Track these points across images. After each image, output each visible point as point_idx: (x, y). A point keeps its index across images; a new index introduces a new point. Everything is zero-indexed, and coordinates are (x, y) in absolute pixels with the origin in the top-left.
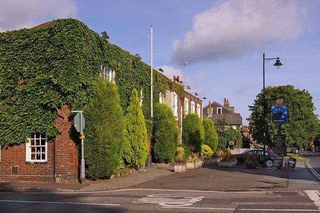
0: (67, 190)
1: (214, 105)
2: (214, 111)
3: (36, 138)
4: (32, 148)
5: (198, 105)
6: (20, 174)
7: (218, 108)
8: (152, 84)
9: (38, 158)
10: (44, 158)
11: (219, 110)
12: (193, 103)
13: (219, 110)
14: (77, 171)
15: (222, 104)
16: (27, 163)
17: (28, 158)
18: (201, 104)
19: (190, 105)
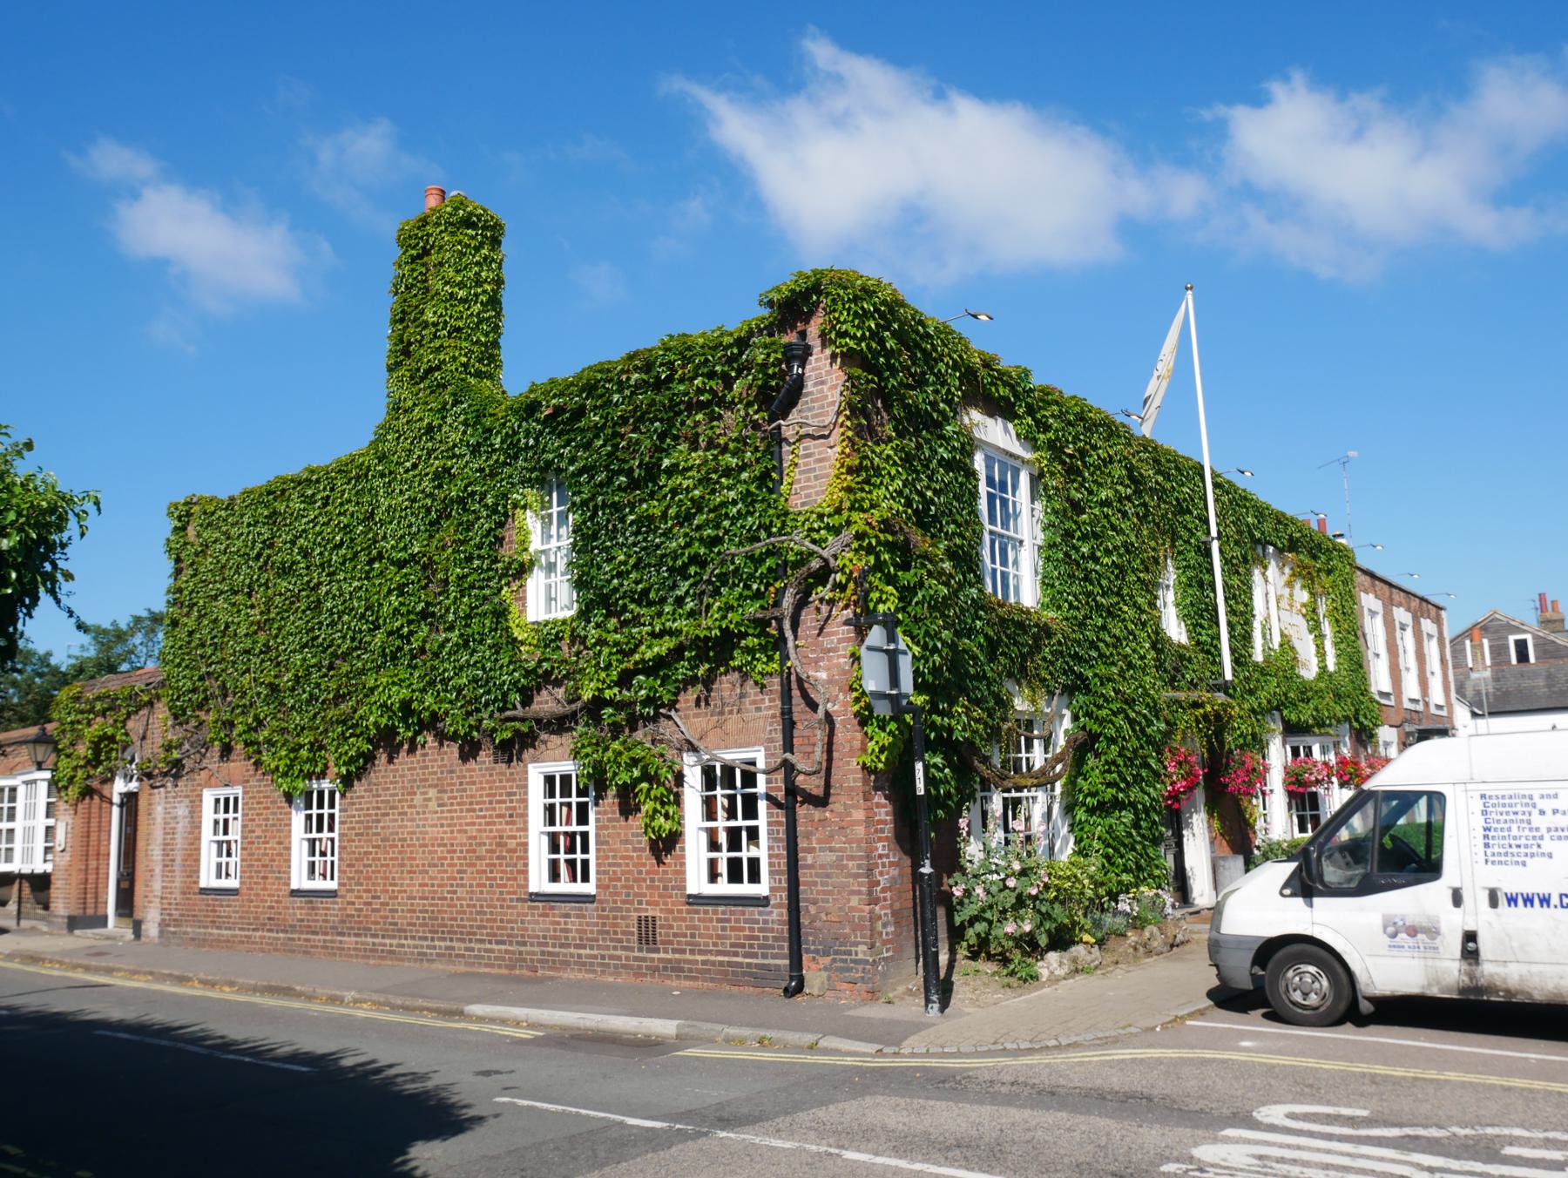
0: (1281, 1062)
1: (1492, 628)
2: (1499, 651)
3: (561, 797)
4: (220, 843)
5: (1428, 626)
6: (666, 951)
7: (1512, 639)
8: (1214, 533)
9: (735, 876)
10: (755, 877)
11: (1521, 646)
12: (1402, 615)
13: (1521, 646)
14: (804, 921)
15: (1530, 618)
16: (698, 900)
17: (539, 881)
18: (1438, 621)
19: (1389, 623)
